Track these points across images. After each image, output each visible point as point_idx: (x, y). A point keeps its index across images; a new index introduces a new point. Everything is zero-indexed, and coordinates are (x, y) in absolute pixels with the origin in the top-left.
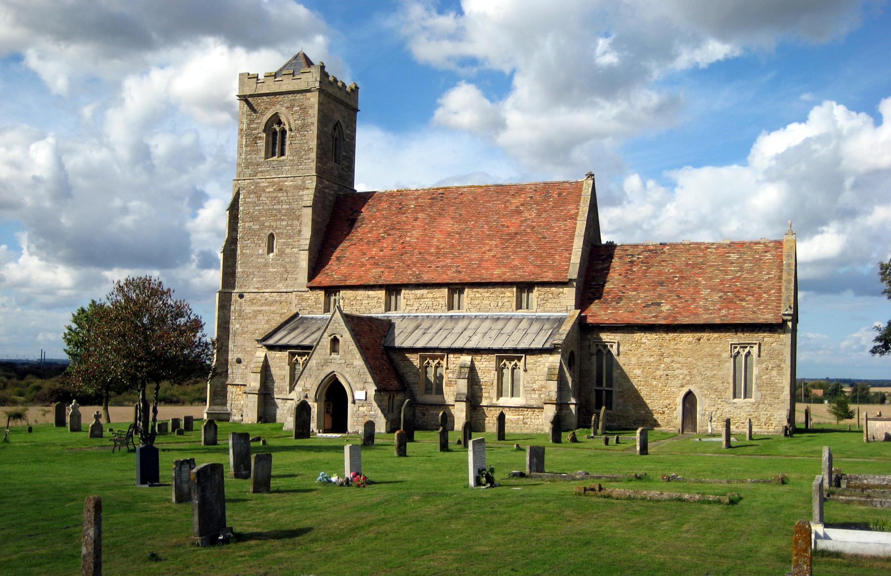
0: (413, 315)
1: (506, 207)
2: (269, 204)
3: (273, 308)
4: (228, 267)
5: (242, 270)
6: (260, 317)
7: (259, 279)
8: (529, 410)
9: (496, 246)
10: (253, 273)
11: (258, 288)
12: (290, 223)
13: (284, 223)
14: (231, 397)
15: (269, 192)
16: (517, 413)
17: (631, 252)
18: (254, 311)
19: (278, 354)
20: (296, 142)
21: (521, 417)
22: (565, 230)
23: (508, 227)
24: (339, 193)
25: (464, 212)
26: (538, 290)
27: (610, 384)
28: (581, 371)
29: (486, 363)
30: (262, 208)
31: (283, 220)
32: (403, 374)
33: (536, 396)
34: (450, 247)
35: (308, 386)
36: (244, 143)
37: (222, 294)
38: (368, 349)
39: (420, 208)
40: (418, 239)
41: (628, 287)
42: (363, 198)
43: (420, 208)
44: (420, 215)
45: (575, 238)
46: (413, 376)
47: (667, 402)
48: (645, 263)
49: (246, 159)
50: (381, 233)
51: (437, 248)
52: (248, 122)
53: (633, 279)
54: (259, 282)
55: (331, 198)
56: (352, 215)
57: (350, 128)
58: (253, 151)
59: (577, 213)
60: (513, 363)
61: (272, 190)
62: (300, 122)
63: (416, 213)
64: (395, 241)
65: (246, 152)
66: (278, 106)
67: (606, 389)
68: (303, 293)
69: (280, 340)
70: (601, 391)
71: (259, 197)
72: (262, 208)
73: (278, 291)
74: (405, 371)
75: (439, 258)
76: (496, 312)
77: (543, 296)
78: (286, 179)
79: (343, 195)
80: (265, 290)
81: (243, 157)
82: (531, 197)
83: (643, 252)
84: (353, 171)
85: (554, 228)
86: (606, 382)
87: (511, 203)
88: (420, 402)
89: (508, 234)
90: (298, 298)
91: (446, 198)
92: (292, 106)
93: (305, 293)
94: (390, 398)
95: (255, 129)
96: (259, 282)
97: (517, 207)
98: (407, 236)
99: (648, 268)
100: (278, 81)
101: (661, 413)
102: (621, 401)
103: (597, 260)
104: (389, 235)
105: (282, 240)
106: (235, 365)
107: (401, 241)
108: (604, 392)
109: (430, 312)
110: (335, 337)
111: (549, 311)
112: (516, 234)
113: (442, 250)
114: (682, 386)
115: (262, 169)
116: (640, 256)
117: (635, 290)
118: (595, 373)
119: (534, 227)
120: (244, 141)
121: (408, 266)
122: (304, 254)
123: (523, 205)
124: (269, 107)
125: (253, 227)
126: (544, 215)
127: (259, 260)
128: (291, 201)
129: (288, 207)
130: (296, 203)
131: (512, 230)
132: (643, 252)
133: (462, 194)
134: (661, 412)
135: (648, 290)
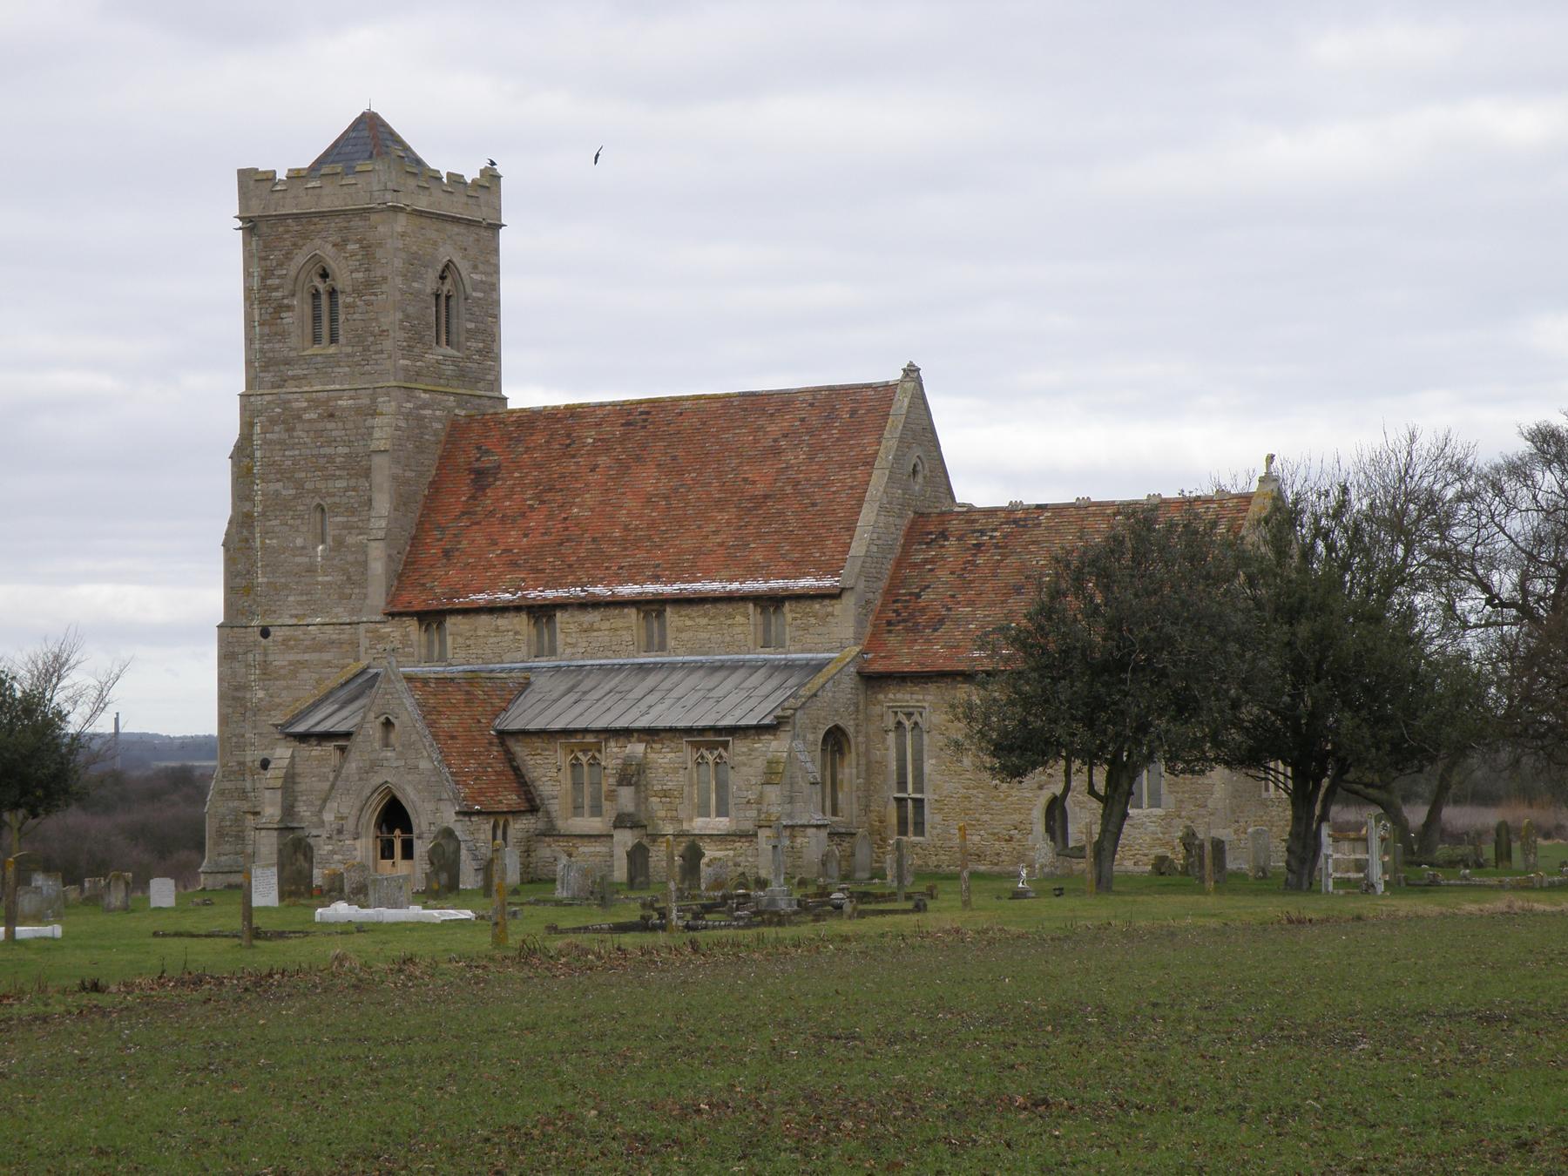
0: (575, 663)
1: (756, 441)
2: (313, 445)
3: (326, 656)
4: (236, 576)
5: (265, 580)
6: (304, 674)
7: (299, 598)
8: (744, 840)
9: (728, 523)
10: (286, 586)
11: (296, 616)
12: (353, 482)
13: (341, 484)
14: (252, 837)
15: (309, 421)
16: (723, 847)
17: (982, 524)
18: (291, 663)
19: (316, 751)
20: (355, 316)
21: (731, 853)
22: (851, 488)
23: (754, 482)
24: (457, 411)
25: (680, 453)
26: (791, 611)
27: (919, 787)
28: (869, 763)
29: (670, 755)
30: (297, 452)
31: (340, 477)
32: (533, 782)
33: (754, 813)
34: (648, 528)
35: (345, 811)
36: (257, 318)
37: (228, 630)
38: (453, 738)
39: (603, 446)
40: (592, 510)
41: (960, 597)
42: (500, 423)
43: (603, 446)
44: (603, 460)
45: (865, 505)
46: (550, 783)
47: (1017, 817)
48: (1000, 547)
49: (261, 350)
50: (530, 499)
51: (626, 528)
52: (263, 274)
53: (971, 582)
54: (300, 603)
55: (438, 426)
56: (478, 460)
57: (481, 267)
58: (276, 334)
59: (877, 452)
60: (716, 753)
61: (314, 416)
62: (361, 275)
63: (596, 456)
64: (550, 517)
65: (262, 336)
66: (318, 242)
67: (913, 796)
68: (379, 626)
69: (318, 723)
70: (905, 800)
71: (290, 430)
72: (297, 452)
73: (335, 620)
74: (535, 774)
75: (626, 549)
76: (720, 654)
77: (799, 622)
78: (341, 393)
79: (466, 416)
80: (309, 621)
81: (257, 346)
82: (802, 420)
83: (1002, 524)
84: (497, 358)
85: (833, 483)
86: (913, 784)
87: (766, 433)
88: (562, 832)
89: (752, 498)
90: (371, 635)
91: (653, 423)
92: (345, 241)
93: (382, 625)
94: (495, 828)
95: (276, 289)
96: (300, 603)
97: (775, 440)
98: (573, 504)
99: (1004, 556)
100: (313, 188)
101: (1006, 840)
102: (938, 818)
103: (920, 544)
104: (542, 502)
105: (339, 519)
106: (259, 774)
107: (563, 515)
108: (910, 803)
109: (607, 657)
110: (387, 719)
111: (810, 651)
112: (766, 497)
113: (634, 533)
114: (1041, 788)
115: (295, 372)
116: (995, 534)
117: (971, 603)
118: (893, 766)
119: (798, 483)
120: (256, 312)
121: (570, 566)
122: (377, 548)
123: (785, 436)
124: (301, 243)
125: (284, 493)
126: (821, 457)
127: (298, 559)
128: (352, 438)
129: (346, 450)
130: (361, 443)
131: (760, 489)
132: (1002, 524)
133: (681, 414)
134: (1007, 837)
135: (992, 604)
